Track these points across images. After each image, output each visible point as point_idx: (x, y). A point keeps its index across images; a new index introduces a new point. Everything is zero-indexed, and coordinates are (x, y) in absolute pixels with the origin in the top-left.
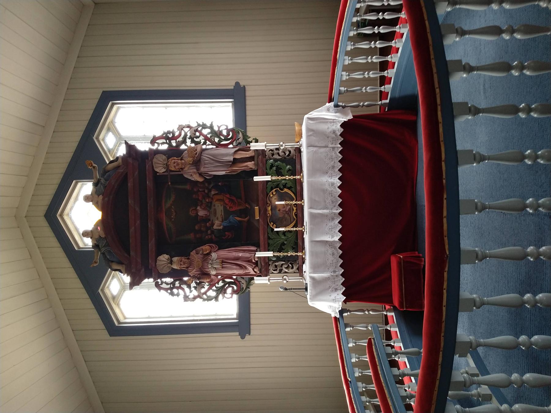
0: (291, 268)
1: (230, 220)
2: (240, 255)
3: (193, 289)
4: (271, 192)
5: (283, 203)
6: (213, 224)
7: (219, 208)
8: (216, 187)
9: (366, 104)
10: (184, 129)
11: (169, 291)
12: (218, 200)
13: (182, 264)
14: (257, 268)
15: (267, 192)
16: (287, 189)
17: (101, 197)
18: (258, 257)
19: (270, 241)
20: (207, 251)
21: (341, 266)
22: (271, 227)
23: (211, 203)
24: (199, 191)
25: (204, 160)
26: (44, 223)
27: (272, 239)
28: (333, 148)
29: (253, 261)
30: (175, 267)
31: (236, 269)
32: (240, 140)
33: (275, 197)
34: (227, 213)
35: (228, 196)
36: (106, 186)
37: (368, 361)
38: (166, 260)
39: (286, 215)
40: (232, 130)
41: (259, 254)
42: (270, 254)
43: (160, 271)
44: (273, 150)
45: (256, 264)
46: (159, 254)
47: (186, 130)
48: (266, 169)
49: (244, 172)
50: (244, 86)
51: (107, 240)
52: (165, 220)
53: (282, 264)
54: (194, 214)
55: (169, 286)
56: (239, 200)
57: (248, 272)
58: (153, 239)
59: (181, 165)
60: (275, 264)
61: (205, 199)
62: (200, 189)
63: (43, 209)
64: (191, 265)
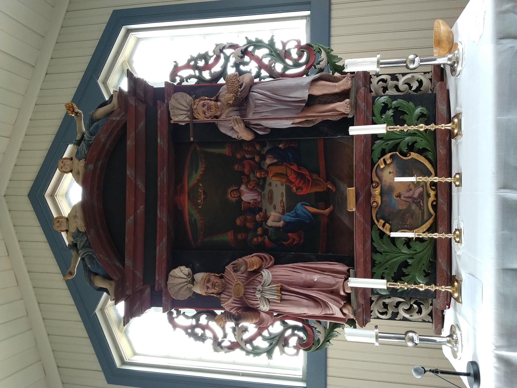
0: (417, 313)
1: (297, 212)
2: (316, 277)
4: (382, 159)
6: (266, 218)
8: (274, 151)
10: (224, 51)
12: (277, 175)
13: (210, 286)
14: (349, 307)
15: (372, 159)
16: (416, 154)
17: (82, 163)
18: (352, 288)
19: (378, 258)
20: (253, 265)
22: (379, 229)
23: (265, 179)
24: (244, 158)
25: (254, 98)
27: (381, 253)
29: (342, 293)
30: (198, 290)
31: (307, 306)
32: (323, 64)
33: (390, 169)
35: (295, 167)
36: (91, 145)
38: (185, 277)
39: (414, 207)
40: (308, 47)
43: (173, 296)
44: (387, 80)
45: (347, 299)
47: (228, 52)
48: (373, 115)
49: (326, 123)
51: (87, 237)
52: (187, 206)
53: (398, 303)
54: (235, 199)
56: (315, 176)
57: (331, 312)
58: (165, 239)
59: (215, 110)
60: (384, 301)
61: (254, 173)
62: (247, 154)
63: (27, 186)
64: (225, 290)
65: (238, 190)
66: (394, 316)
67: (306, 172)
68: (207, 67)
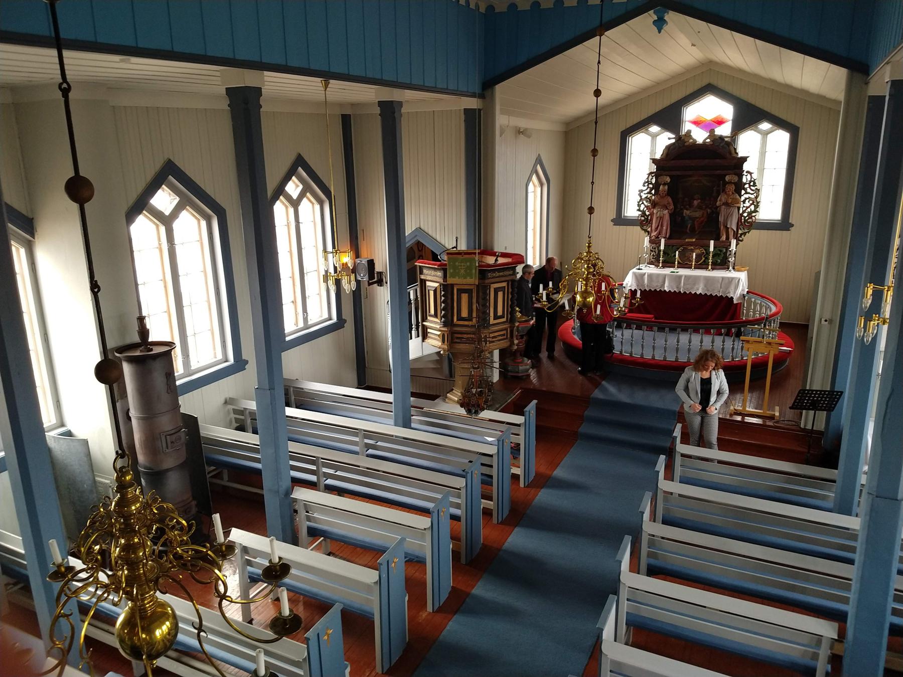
2: (664, 228)
3: (646, 195)
5: (694, 257)
6: (687, 210)
7: (698, 214)
9: (745, 311)
11: (647, 180)
19: (671, 247)
21: (650, 290)
26: (704, 82)
28: (720, 291)
30: (661, 187)
34: (693, 219)
37: (568, 300)
39: (686, 258)
41: (663, 241)
42: (662, 247)
46: (671, 177)
50: (789, 230)
55: (650, 180)
65: (698, 199)
66: (651, 251)
67: (703, 224)
68: (750, 186)
